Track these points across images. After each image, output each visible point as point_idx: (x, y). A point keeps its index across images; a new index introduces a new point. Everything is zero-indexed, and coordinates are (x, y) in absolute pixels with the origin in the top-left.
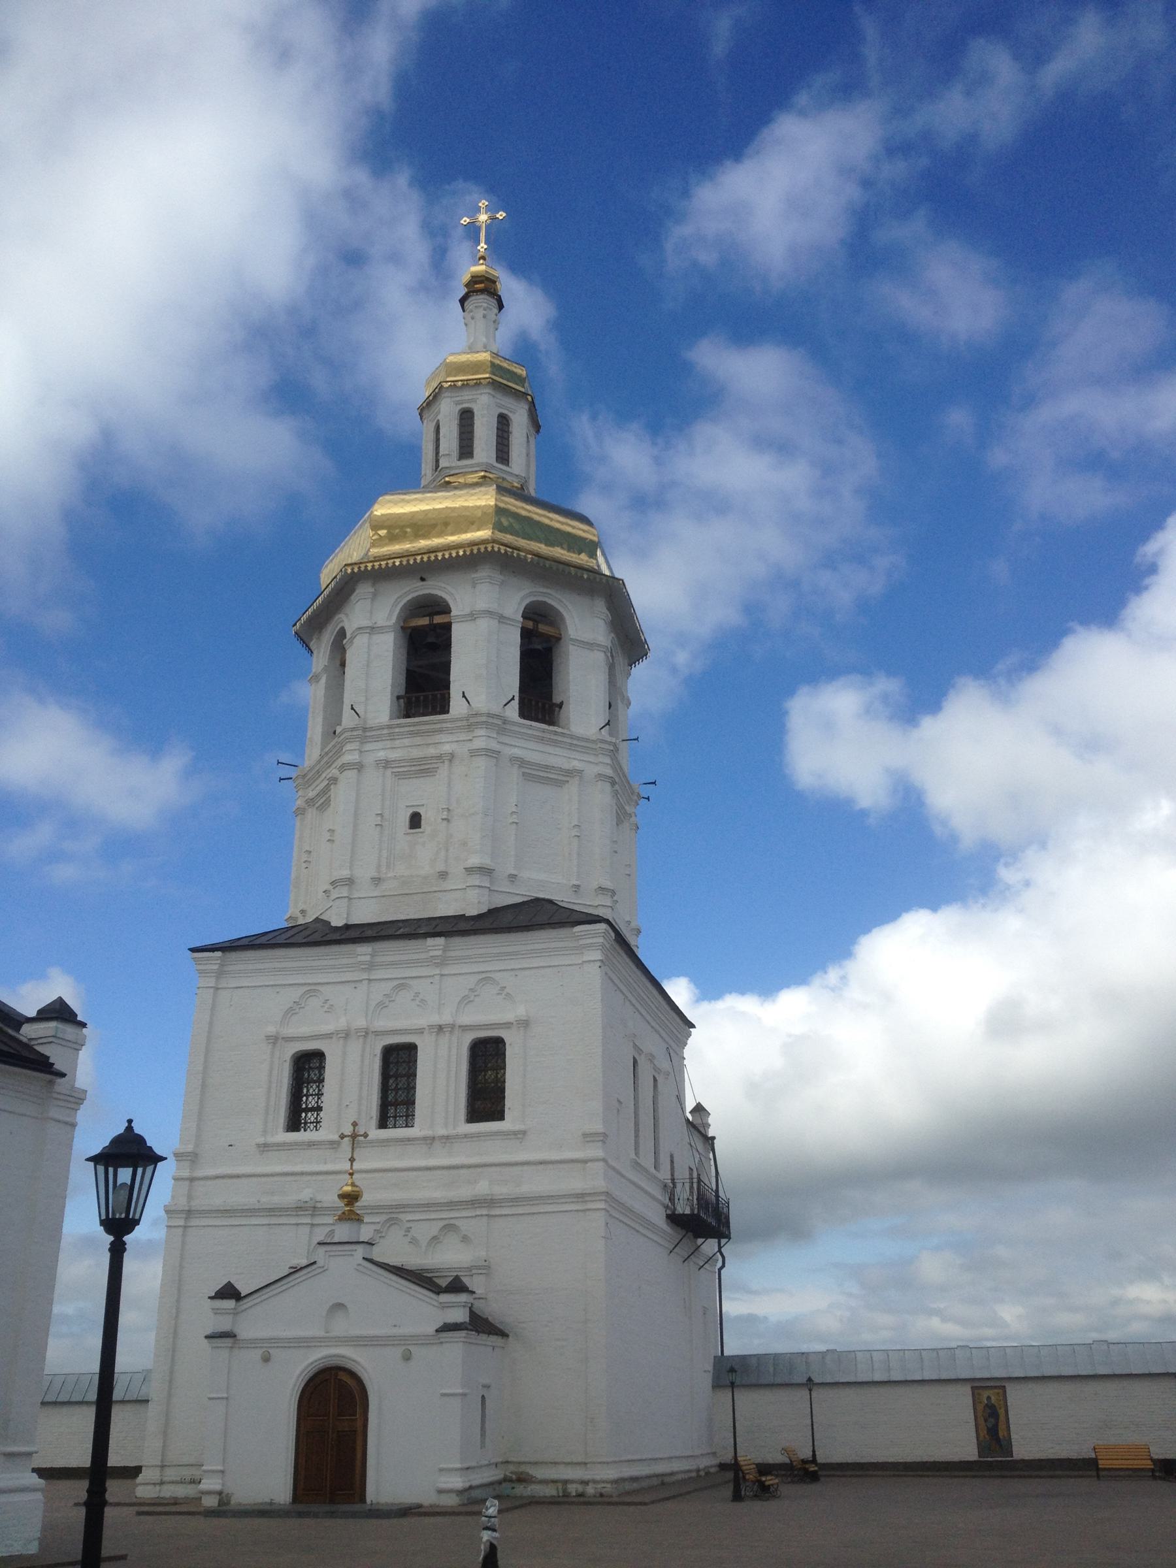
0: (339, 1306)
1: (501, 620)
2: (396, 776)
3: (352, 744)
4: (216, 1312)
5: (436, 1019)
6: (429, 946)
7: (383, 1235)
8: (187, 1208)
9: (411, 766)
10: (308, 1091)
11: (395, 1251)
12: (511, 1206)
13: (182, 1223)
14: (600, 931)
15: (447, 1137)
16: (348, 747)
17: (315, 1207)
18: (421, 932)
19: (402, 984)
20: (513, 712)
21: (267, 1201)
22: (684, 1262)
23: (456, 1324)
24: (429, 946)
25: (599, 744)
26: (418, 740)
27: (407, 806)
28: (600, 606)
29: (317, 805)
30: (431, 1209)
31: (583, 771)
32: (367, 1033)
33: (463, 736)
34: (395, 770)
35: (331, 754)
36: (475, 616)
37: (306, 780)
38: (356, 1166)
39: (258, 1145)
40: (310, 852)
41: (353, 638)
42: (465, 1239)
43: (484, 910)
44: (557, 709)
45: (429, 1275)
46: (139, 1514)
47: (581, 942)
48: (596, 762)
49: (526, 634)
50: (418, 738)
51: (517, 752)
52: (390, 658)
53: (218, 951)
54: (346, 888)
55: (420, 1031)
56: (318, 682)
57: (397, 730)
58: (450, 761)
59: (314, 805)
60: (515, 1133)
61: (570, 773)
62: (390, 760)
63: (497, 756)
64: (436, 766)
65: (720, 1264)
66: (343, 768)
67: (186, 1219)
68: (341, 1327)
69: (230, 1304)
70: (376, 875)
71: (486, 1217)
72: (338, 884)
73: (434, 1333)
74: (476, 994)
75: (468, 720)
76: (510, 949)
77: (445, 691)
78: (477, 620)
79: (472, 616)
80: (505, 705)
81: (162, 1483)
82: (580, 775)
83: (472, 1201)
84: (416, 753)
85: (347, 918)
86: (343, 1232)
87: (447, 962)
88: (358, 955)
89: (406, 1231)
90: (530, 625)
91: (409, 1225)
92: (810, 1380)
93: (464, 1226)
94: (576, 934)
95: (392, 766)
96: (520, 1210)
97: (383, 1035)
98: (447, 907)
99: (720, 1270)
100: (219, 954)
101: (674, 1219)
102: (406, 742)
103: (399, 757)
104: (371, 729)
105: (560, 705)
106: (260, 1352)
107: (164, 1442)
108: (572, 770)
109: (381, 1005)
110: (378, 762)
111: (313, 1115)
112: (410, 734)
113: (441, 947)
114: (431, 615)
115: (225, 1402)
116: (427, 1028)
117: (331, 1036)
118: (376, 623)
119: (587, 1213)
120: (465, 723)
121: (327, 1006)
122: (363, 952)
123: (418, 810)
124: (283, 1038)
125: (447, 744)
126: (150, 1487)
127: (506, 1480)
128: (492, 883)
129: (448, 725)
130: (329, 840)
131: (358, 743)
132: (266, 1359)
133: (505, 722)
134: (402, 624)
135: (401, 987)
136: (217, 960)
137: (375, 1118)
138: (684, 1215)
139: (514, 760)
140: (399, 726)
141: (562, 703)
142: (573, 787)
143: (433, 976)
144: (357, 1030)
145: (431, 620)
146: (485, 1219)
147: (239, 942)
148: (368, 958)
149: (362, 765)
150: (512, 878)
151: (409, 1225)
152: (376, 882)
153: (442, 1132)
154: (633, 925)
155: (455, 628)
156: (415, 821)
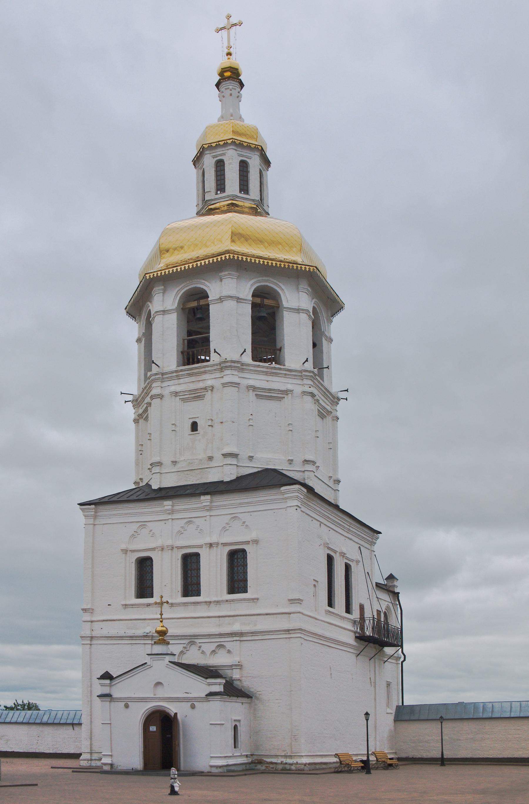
0: (159, 684)
1: (239, 301)
2: (182, 400)
3: (156, 383)
4: (102, 685)
5: (208, 540)
6: (202, 500)
7: (188, 649)
8: (90, 636)
9: (190, 394)
10: (191, 560)
11: (191, 659)
12: (252, 636)
13: (89, 642)
14: (295, 489)
15: (218, 602)
16: (154, 385)
17: (153, 636)
18: (197, 492)
19: (190, 521)
20: (248, 358)
21: (130, 633)
22: (370, 660)
23: (216, 692)
24: (202, 500)
25: (303, 372)
26: (193, 379)
27: (189, 418)
28: (304, 285)
29: (144, 417)
30: (211, 637)
31: (293, 390)
32: (173, 548)
33: (218, 375)
34: (181, 397)
35: (147, 388)
36: (222, 300)
37: (138, 402)
38: (163, 616)
39: (123, 605)
40: (143, 445)
41: (154, 318)
42: (229, 652)
43: (233, 477)
44: (278, 352)
45: (211, 669)
46: (73, 771)
47: (286, 496)
48: (302, 384)
49: (254, 306)
50: (193, 377)
51: (251, 382)
52: (175, 329)
53: (92, 505)
54: (158, 467)
55: (201, 547)
56: (141, 342)
57: (180, 373)
58: (212, 390)
59: (142, 418)
60: (253, 599)
61: (286, 392)
62: (178, 391)
63: (238, 386)
64: (203, 393)
65: (402, 659)
66: (152, 398)
67: (91, 640)
68: (161, 693)
69: (108, 682)
70: (174, 460)
71: (239, 641)
72: (154, 465)
73: (205, 696)
74: (230, 526)
75: (221, 365)
76: (246, 501)
77: (207, 347)
78: (223, 301)
79: (221, 300)
80: (242, 354)
81: (91, 760)
82: (291, 393)
83: (231, 633)
84: (192, 386)
85: (160, 485)
86: (158, 649)
87: (213, 509)
88: (165, 506)
89: (199, 648)
90: (258, 300)
91: (200, 645)
92: (441, 717)
93: (228, 645)
94: (282, 491)
95: (180, 395)
96: (256, 638)
97: (182, 548)
98: (213, 477)
99: (402, 662)
100: (93, 506)
101: (361, 638)
102: (187, 380)
103: (183, 389)
104: (166, 373)
105: (280, 350)
106: (123, 703)
107: (91, 742)
108: (286, 390)
109: (180, 533)
110: (172, 393)
111: (241, 560)
112: (189, 375)
113: (209, 501)
114: (198, 299)
115: (109, 725)
116: (204, 545)
117: (155, 549)
118: (166, 308)
119: (291, 639)
120: (219, 367)
121: (151, 533)
122: (168, 504)
123: (196, 421)
124: (130, 551)
125: (209, 380)
126: (86, 762)
127: (252, 762)
128: (238, 461)
129: (209, 369)
130: (149, 440)
131: (159, 382)
132: (127, 706)
133: (243, 364)
134: (182, 307)
135: (190, 522)
136: (93, 509)
137: (180, 591)
138: (370, 636)
139: (249, 387)
140: (181, 371)
141: (281, 348)
142: (288, 400)
143: (206, 516)
144: (168, 546)
145: (198, 303)
146: (238, 642)
147: (104, 499)
148: (170, 507)
149: (163, 395)
150: (251, 458)
151: (200, 645)
152: (174, 464)
153: (215, 599)
154: (334, 478)
155: (211, 307)
156: (194, 427)
